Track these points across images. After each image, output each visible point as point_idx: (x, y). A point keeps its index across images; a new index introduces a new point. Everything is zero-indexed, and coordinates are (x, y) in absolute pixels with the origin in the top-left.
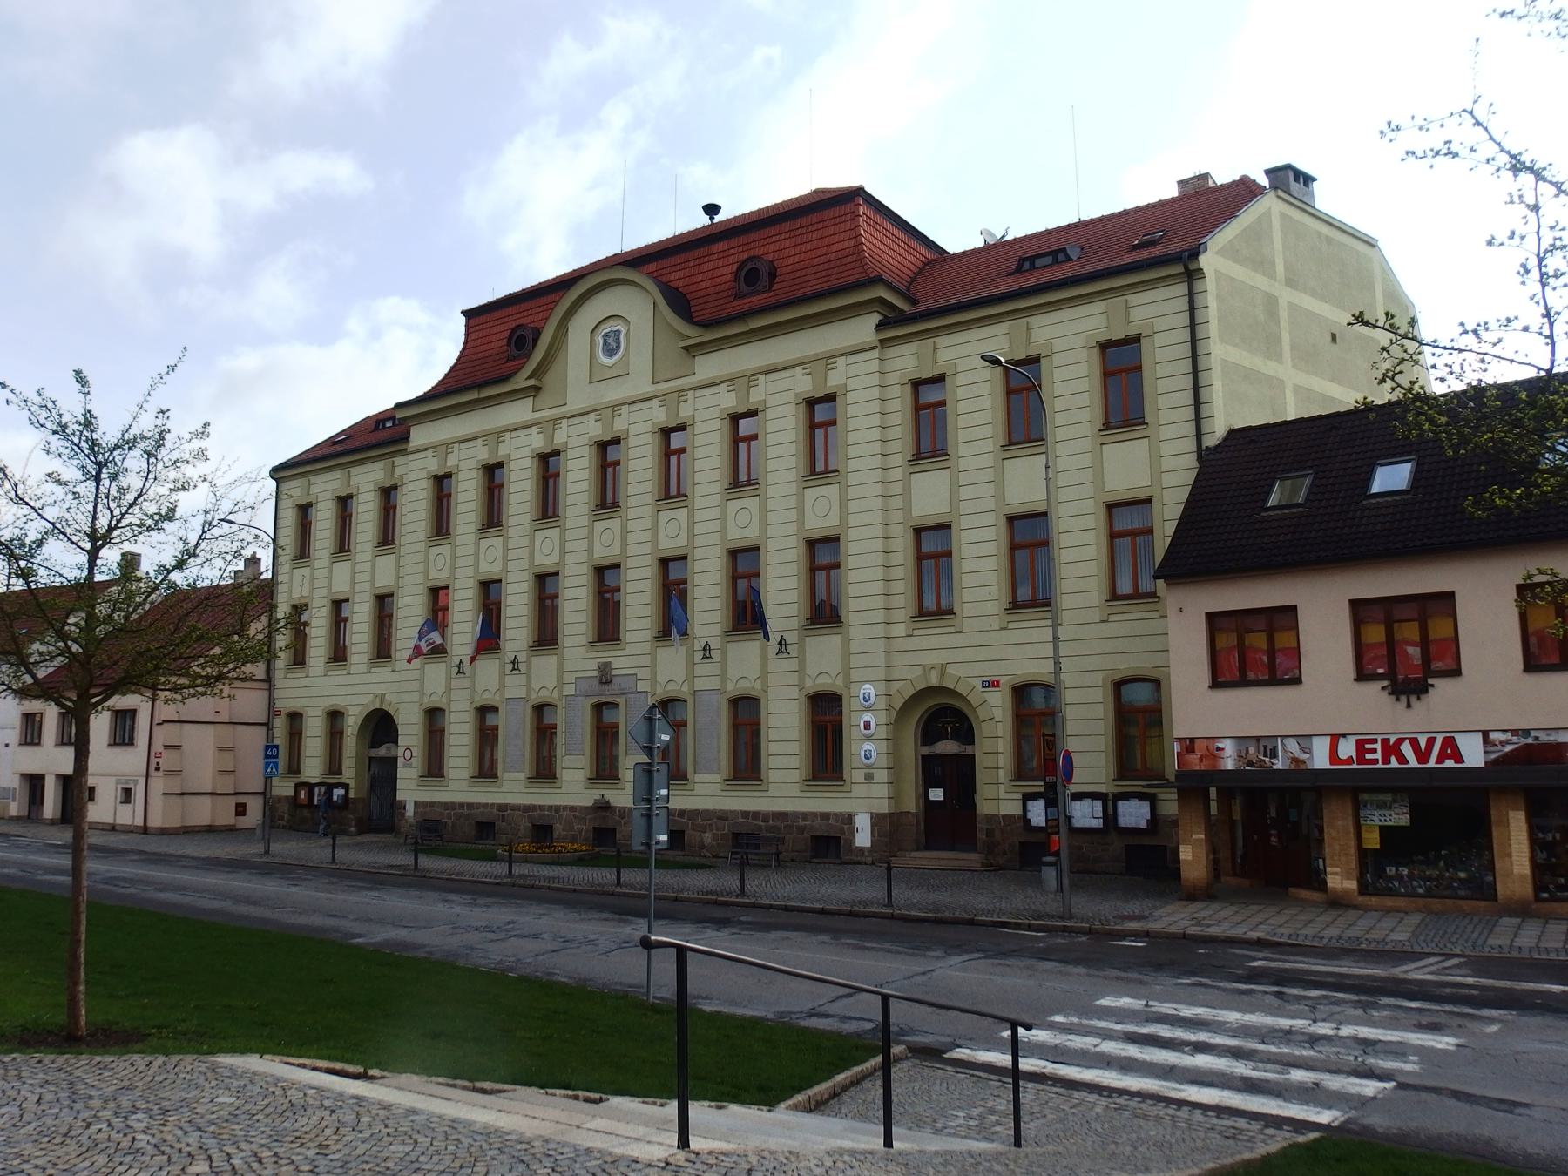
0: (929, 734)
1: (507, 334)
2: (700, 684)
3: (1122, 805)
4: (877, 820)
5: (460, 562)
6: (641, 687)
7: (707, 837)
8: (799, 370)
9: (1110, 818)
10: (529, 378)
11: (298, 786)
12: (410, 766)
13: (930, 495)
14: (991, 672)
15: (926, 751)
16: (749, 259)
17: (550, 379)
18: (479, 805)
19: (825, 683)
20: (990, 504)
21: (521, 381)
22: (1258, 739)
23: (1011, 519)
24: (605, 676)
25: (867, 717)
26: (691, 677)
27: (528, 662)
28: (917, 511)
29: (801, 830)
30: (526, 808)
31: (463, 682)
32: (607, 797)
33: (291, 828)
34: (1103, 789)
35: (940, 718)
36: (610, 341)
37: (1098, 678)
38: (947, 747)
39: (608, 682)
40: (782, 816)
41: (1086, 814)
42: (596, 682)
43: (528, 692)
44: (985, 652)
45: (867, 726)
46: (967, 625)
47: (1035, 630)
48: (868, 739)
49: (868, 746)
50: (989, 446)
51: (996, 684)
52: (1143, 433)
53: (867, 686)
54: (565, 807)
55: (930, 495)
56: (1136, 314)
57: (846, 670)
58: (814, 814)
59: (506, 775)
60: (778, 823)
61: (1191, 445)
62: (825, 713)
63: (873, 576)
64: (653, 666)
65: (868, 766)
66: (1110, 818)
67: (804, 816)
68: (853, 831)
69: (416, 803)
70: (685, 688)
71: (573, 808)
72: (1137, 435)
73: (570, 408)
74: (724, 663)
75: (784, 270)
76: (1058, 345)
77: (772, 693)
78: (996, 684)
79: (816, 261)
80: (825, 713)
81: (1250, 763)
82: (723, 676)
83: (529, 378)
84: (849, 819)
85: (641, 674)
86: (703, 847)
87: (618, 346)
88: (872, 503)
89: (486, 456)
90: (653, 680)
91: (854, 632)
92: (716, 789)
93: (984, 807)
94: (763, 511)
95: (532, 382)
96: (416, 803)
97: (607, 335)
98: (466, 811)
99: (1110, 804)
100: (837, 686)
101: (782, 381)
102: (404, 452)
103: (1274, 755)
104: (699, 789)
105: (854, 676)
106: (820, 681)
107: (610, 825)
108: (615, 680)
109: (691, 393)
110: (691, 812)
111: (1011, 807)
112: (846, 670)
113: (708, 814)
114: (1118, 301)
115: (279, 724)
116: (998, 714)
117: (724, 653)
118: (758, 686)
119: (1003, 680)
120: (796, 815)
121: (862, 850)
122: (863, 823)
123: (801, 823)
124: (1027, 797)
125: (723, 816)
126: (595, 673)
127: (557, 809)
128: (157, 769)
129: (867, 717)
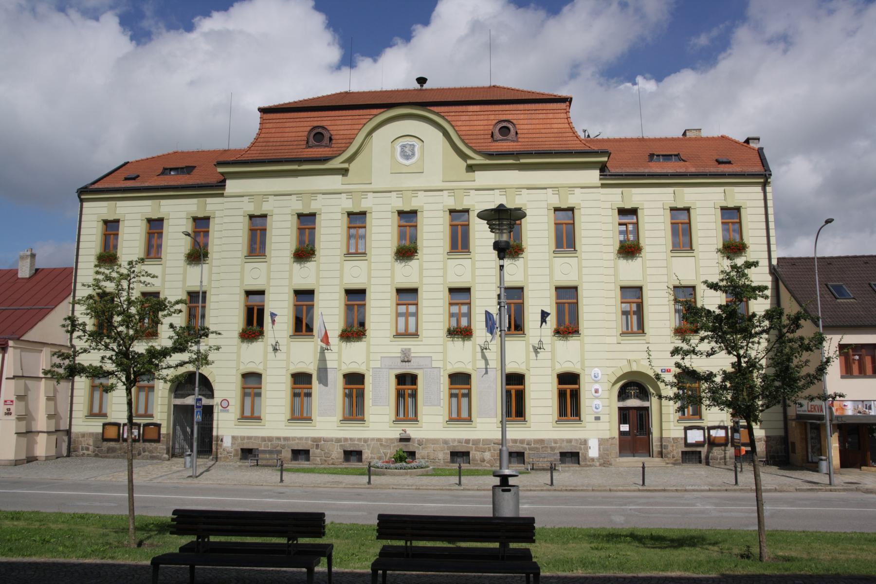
0: (623, 394)
1: (309, 128)
4: (602, 442)
7: (487, 455)
8: (294, 197)
10: (343, 162)
12: (228, 411)
15: (622, 404)
16: (508, 121)
17: (353, 167)
18: (294, 439)
20: (440, 280)
21: (335, 164)
22: (863, 401)
25: (597, 386)
29: (553, 449)
30: (338, 440)
33: (96, 456)
36: (407, 150)
40: (541, 441)
42: (399, 360)
43: (340, 365)
45: (597, 391)
47: (635, 344)
50: (239, 254)
53: (596, 369)
54: (373, 439)
55: (256, 275)
58: (563, 440)
59: (478, 420)
60: (537, 446)
62: (569, 383)
64: (445, 352)
65: (597, 413)
67: (555, 441)
68: (587, 448)
69: (234, 438)
71: (379, 440)
73: (374, 186)
74: (288, 353)
75: (337, 137)
76: (127, 217)
79: (543, 131)
80: (569, 383)
81: (860, 412)
83: (343, 162)
84: (585, 442)
86: (483, 461)
87: (413, 154)
89: (252, 209)
90: (444, 360)
91: (587, 340)
94: (269, 271)
95: (345, 166)
96: (234, 438)
97: (403, 146)
98: (283, 442)
101: (382, 198)
102: (222, 195)
103: (870, 408)
105: (587, 363)
108: (413, 360)
110: (473, 440)
112: (582, 361)
120: (549, 441)
121: (593, 460)
123: (553, 445)
126: (399, 355)
127: (366, 440)
129: (597, 386)
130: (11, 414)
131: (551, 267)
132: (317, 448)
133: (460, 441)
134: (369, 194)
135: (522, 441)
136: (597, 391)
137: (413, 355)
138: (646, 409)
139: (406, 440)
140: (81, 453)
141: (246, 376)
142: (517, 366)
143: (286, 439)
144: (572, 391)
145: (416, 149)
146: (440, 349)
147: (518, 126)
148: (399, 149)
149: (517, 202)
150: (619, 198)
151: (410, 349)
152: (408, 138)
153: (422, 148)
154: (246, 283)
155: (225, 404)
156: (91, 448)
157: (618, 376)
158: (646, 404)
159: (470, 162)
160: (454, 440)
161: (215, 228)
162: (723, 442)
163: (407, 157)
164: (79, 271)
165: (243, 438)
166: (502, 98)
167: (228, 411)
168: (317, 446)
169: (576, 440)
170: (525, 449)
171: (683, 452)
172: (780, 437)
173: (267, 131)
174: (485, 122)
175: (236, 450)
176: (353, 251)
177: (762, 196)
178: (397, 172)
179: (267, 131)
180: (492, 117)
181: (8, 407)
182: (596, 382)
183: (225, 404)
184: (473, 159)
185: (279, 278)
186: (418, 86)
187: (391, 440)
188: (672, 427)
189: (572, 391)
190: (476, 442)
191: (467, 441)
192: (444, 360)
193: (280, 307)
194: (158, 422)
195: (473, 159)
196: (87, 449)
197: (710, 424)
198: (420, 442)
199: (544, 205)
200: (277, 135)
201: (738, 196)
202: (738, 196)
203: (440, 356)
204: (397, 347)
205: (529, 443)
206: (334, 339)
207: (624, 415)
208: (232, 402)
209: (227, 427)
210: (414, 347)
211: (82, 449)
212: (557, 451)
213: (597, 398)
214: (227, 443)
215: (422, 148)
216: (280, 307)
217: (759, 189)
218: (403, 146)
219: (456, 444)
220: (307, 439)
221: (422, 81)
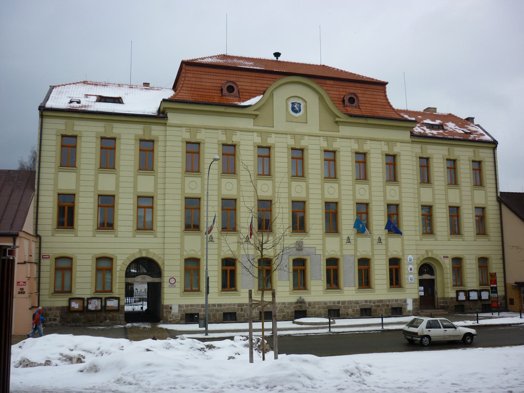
2: (345, 253)
3: (470, 293)
4: (414, 301)
5: (216, 187)
6: (318, 252)
9: (480, 297)
11: (71, 300)
12: (175, 287)
13: (146, 184)
14: (446, 253)
15: (421, 277)
18: (225, 305)
19: (228, 254)
23: (59, 194)
24: (299, 247)
25: (411, 266)
26: (341, 250)
27: (386, 240)
28: (99, 189)
29: (388, 306)
31: (351, 246)
32: (302, 298)
34: (476, 289)
35: (426, 268)
36: (295, 106)
37: (474, 257)
38: (427, 276)
39: (302, 250)
40: (381, 301)
41: (474, 296)
44: (443, 247)
45: (411, 269)
46: (120, 234)
47: (456, 241)
48: (410, 275)
49: (411, 276)
51: (447, 257)
52: (75, 171)
56: (76, 128)
57: (403, 250)
58: (393, 300)
59: (345, 288)
60: (379, 304)
61: (495, 194)
62: (395, 264)
63: (410, 220)
64: (324, 245)
66: (480, 297)
67: (389, 301)
68: (406, 305)
70: (339, 254)
72: (73, 171)
74: (356, 245)
77: (376, 257)
78: (447, 257)
80: (395, 264)
82: (356, 249)
84: (405, 301)
85: (318, 247)
87: (300, 110)
88: (409, 195)
90: (324, 250)
91: (405, 238)
92: (353, 292)
93: (439, 294)
97: (293, 104)
99: (103, 302)
100: (198, 255)
104: (346, 293)
106: (363, 253)
107: (304, 309)
108: (304, 249)
109: (338, 139)
111: (453, 295)
112: (403, 250)
113: (350, 302)
114: (69, 121)
115: (47, 266)
116: (448, 266)
117: (356, 241)
118: (370, 254)
119: (449, 256)
120: (386, 301)
121: (409, 312)
122: (410, 302)
123: (388, 303)
124: (458, 292)
125: (357, 302)
128: (22, 292)
129: (411, 266)
130: (24, 293)
131: (385, 192)
132: (242, 311)
133: (334, 302)
134: (202, 129)
135: (370, 301)
136: (411, 269)
137: (304, 246)
138: (433, 280)
139: (301, 302)
140: (50, 323)
141: (188, 260)
142: (334, 253)
143: (219, 305)
144: (231, 271)
145: (302, 106)
146: (321, 242)
147: (240, 87)
148: (290, 106)
149: (394, 151)
150: (63, 127)
151: (302, 242)
152: (296, 99)
153: (306, 106)
154: (99, 189)
155: (172, 281)
156: (58, 319)
157: (132, 260)
158: (433, 277)
159: (337, 119)
160: (330, 302)
161: (159, 148)
162: (117, 308)
163: (296, 112)
164: (41, 175)
165: (187, 306)
166: (297, 72)
167: (175, 287)
168: (242, 310)
169: (400, 300)
170: (372, 306)
171: (455, 306)
172: (67, 307)
173: (189, 79)
174: (337, 93)
175: (182, 315)
176: (261, 173)
177: (492, 155)
178: (289, 120)
179: (189, 79)
180: (225, 78)
181: (22, 287)
182: (410, 264)
183: (172, 281)
184: (339, 117)
185: (212, 188)
186: (275, 59)
187: (292, 303)
188: (450, 291)
189: (231, 271)
190: (344, 302)
191: (339, 302)
192: (324, 250)
193: (211, 212)
194: (117, 296)
195: (339, 117)
196: (55, 320)
197: (469, 289)
198: (310, 304)
199: (180, 139)
200: (197, 83)
201: (481, 155)
202: (76, 128)
203: (320, 247)
204: (291, 240)
205: (374, 302)
206: (215, 233)
207: (422, 283)
208: (178, 279)
209: (173, 297)
210: (269, 240)
211: (50, 320)
212: (390, 307)
213: (411, 274)
214: (175, 310)
215: (306, 106)
216: (211, 212)
217: (491, 151)
218: (293, 104)
219: (331, 304)
220: (234, 304)
221: (277, 55)
